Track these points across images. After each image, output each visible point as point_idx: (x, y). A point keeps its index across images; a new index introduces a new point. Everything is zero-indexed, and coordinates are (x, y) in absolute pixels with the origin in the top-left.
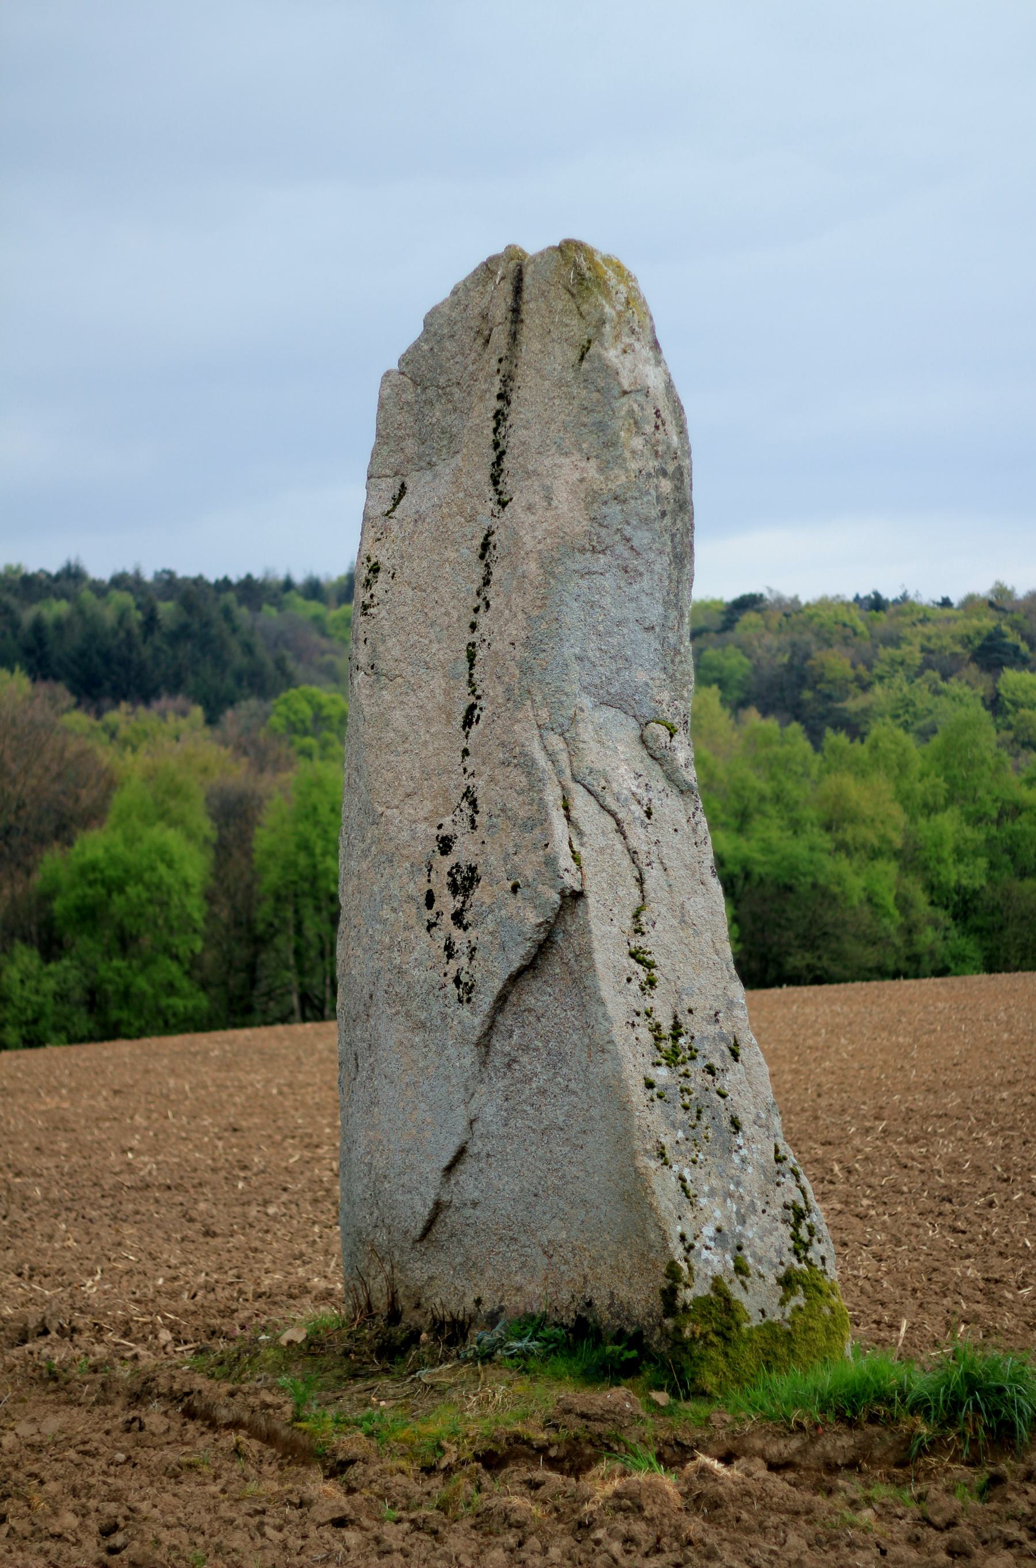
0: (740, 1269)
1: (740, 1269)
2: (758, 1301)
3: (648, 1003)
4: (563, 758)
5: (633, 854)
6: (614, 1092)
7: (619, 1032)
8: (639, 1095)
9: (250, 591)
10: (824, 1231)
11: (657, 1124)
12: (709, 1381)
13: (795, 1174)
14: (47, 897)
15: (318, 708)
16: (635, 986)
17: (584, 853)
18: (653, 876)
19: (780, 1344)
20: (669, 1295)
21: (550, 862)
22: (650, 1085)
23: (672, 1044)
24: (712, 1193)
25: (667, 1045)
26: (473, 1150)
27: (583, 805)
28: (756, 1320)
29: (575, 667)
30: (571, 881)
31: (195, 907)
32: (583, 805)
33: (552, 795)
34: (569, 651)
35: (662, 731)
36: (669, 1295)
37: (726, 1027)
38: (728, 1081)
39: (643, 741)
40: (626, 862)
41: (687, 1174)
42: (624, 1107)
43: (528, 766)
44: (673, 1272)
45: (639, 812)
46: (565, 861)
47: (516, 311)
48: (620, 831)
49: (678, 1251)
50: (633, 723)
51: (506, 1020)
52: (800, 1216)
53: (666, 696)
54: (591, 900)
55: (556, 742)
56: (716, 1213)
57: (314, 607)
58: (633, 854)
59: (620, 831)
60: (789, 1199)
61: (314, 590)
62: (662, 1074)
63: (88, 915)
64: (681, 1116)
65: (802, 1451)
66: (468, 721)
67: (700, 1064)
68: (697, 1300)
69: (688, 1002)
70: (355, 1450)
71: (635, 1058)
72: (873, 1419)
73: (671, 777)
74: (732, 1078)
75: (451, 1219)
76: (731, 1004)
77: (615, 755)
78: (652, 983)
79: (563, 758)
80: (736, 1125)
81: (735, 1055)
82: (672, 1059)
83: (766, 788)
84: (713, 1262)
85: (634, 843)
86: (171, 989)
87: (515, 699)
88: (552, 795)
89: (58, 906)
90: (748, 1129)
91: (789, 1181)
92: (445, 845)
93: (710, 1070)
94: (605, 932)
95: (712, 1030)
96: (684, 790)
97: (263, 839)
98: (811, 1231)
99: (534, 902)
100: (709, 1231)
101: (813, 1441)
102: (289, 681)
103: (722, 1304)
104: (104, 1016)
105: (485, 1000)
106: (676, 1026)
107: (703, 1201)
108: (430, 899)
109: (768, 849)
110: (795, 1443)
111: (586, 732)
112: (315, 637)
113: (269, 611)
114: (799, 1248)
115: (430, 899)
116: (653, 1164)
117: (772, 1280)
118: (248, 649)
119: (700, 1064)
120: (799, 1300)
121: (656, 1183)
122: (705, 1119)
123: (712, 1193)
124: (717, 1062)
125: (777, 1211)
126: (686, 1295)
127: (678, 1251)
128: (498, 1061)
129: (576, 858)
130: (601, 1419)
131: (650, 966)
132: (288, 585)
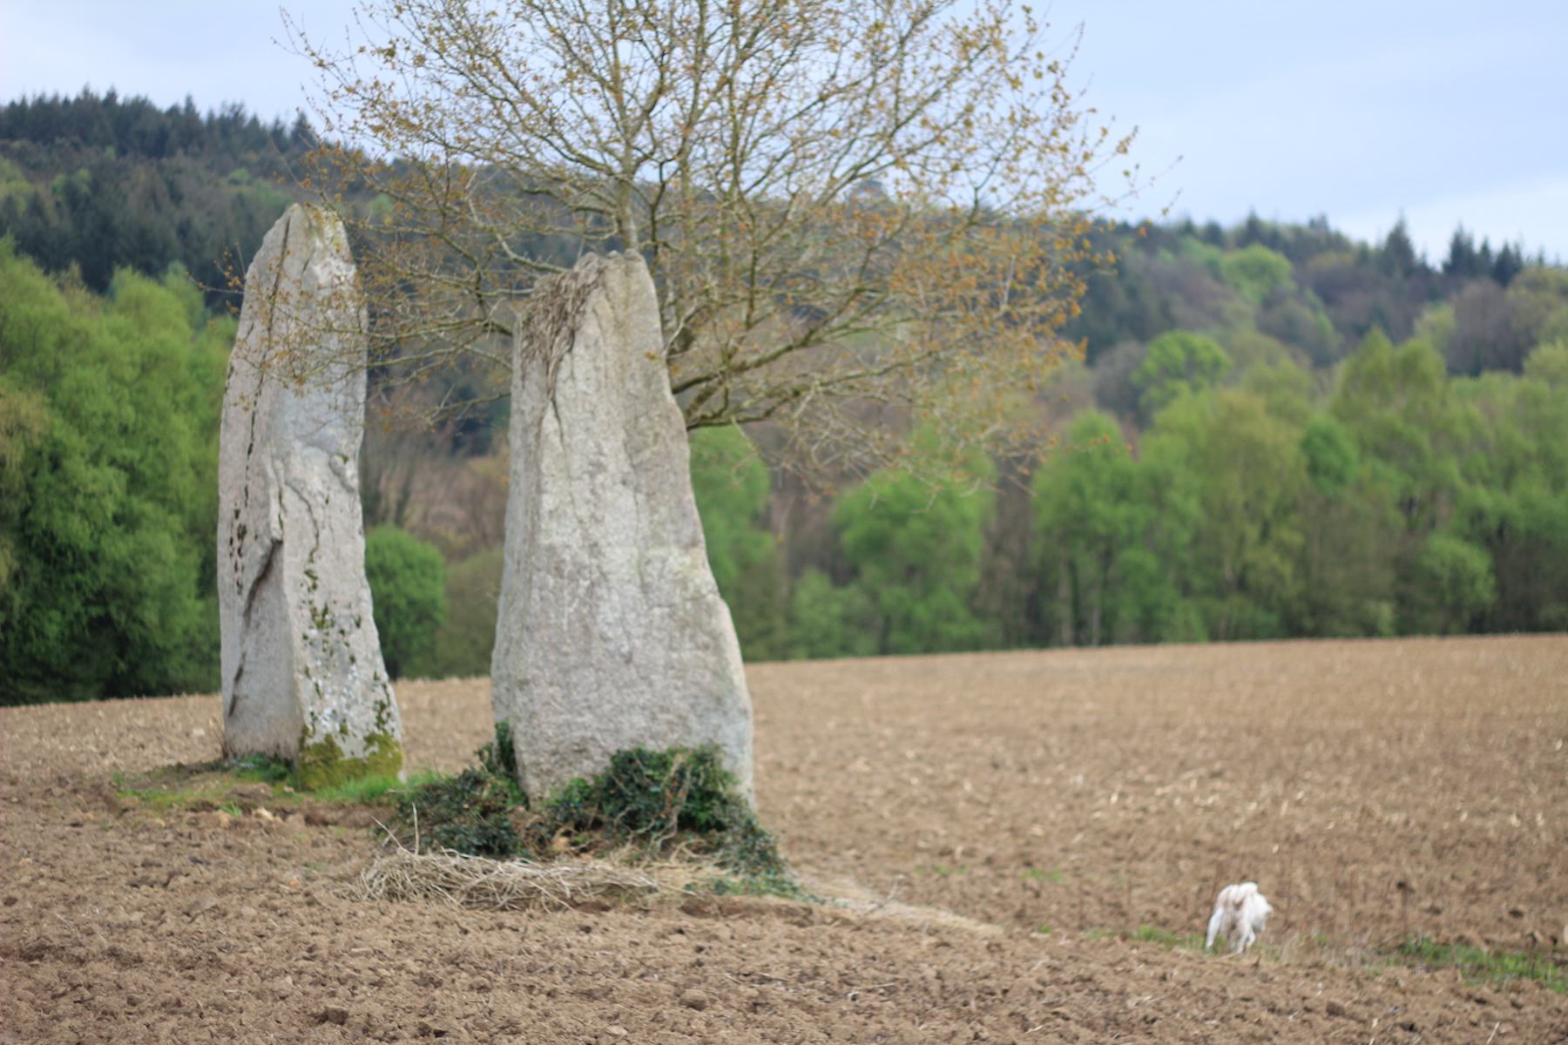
0: (343, 731)
1: (343, 731)
2: (351, 748)
3: (311, 597)
4: (282, 473)
5: (315, 522)
6: (288, 639)
7: (292, 611)
8: (298, 642)
9: (1148, 236)
10: (396, 714)
11: (305, 656)
12: (314, 783)
13: (385, 687)
14: (839, 529)
15: (1191, 352)
16: (305, 588)
17: (285, 521)
18: (324, 534)
19: (358, 768)
20: (302, 741)
21: (268, 525)
22: (305, 637)
23: (321, 619)
24: (333, 693)
25: (319, 618)
26: (246, 668)
27: (289, 496)
28: (348, 756)
29: (291, 427)
30: (276, 535)
31: (975, 544)
32: (289, 496)
33: (273, 491)
34: (288, 418)
35: (339, 460)
36: (302, 741)
37: (355, 611)
38: (351, 638)
39: (330, 465)
40: (310, 526)
41: (320, 683)
42: (290, 648)
43: (264, 475)
44: (305, 731)
45: (321, 500)
46: (275, 525)
47: (285, 240)
48: (309, 509)
49: (308, 720)
50: (325, 455)
51: (256, 604)
52: (383, 707)
53: (344, 442)
54: (286, 545)
55: (279, 464)
56: (333, 702)
57: (1211, 252)
58: (315, 522)
59: (309, 509)
60: (379, 698)
61: (1213, 234)
62: (314, 633)
63: (877, 546)
64: (321, 654)
65: (344, 818)
66: (250, 452)
67: (336, 628)
68: (315, 745)
69: (334, 597)
70: (130, 804)
71: (299, 623)
72: (380, 804)
73: (343, 484)
74: (354, 637)
75: (240, 704)
76: (359, 600)
77: (313, 472)
78: (315, 587)
79: (282, 473)
80: (353, 660)
81: (358, 625)
82: (321, 625)
83: (1531, 445)
84: (327, 726)
85: (316, 516)
86: (950, 618)
87: (264, 442)
88: (273, 491)
89: (848, 538)
90: (359, 661)
91: (380, 690)
92: (237, 513)
93: (342, 632)
94: (291, 564)
95: (346, 612)
96: (350, 490)
97: (1042, 482)
98: (389, 715)
99: (262, 544)
100: (328, 711)
101: (350, 812)
102: (1170, 321)
103: (328, 750)
104: (892, 635)
105: (246, 593)
106: (326, 611)
107: (327, 697)
108: (231, 541)
109: (1527, 504)
110: (340, 814)
111: (295, 461)
112: (1208, 282)
113: (1165, 256)
114: (380, 722)
115: (231, 541)
116: (301, 676)
117: (360, 737)
118: (1132, 293)
119: (336, 628)
120: (375, 748)
121: (301, 687)
122: (335, 656)
123: (333, 693)
124: (346, 628)
125: (370, 704)
126: (309, 742)
127: (308, 720)
128: (253, 624)
129: (281, 523)
130: (248, 796)
131: (315, 578)
132: (1188, 229)
